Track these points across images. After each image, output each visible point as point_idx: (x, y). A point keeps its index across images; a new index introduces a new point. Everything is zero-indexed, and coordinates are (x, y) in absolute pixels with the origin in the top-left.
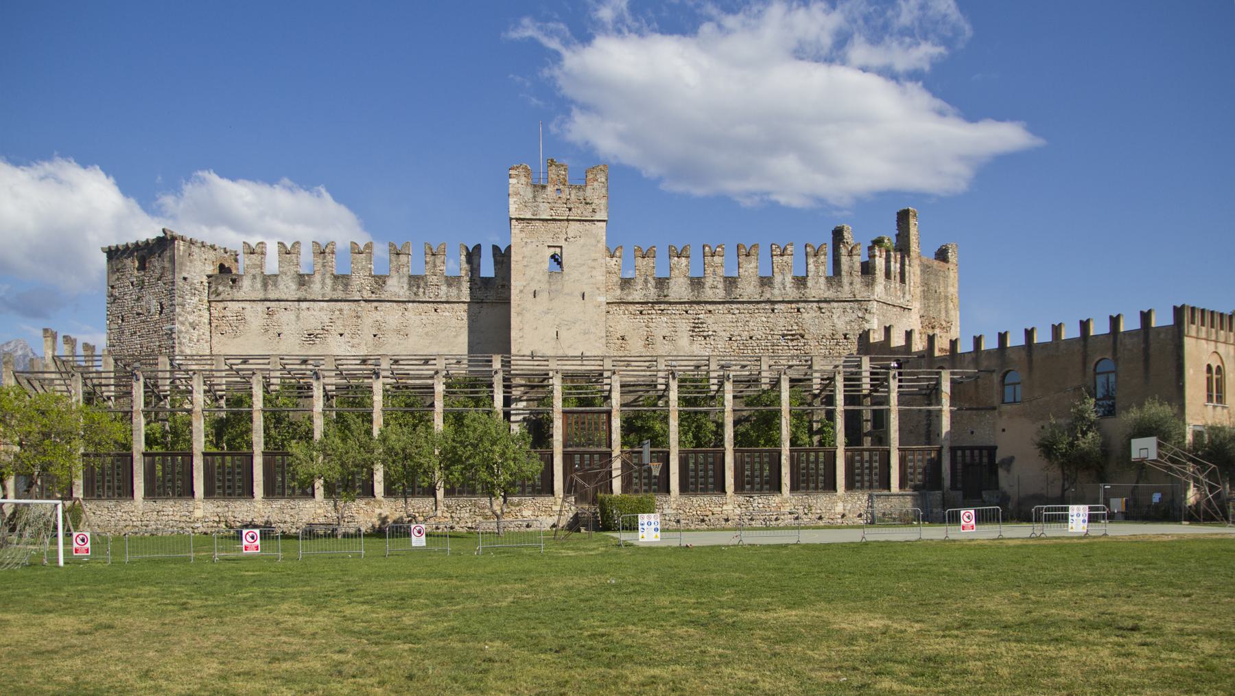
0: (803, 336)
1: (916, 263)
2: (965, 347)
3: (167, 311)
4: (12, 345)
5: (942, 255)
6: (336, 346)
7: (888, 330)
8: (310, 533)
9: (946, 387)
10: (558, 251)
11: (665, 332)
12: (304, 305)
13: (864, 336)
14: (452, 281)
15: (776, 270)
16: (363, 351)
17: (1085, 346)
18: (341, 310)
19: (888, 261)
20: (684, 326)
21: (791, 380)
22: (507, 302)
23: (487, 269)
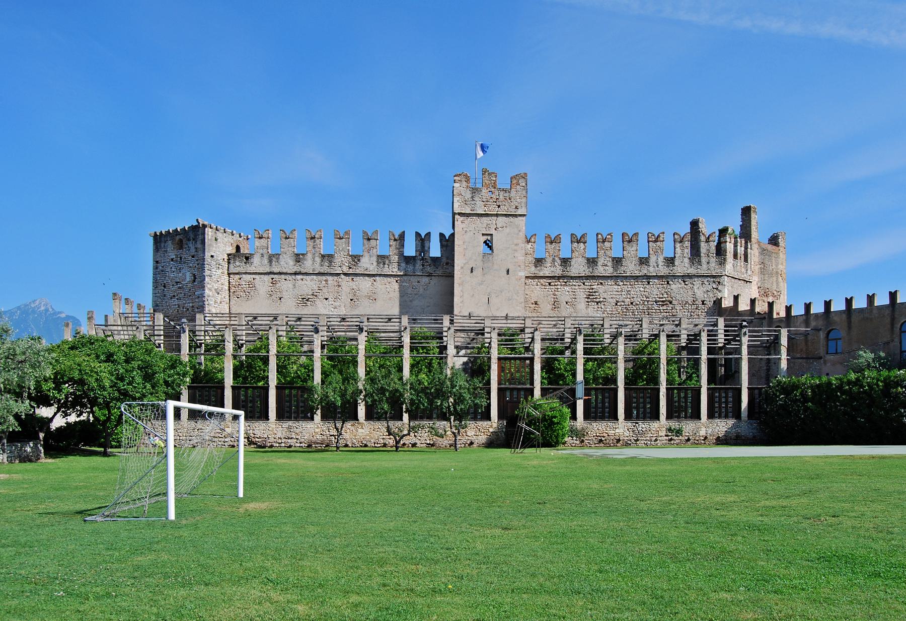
0: (671, 303)
1: (755, 246)
2: (798, 311)
3: (199, 280)
4: (37, 302)
5: (774, 240)
6: (322, 308)
7: (736, 298)
8: (310, 448)
9: (784, 341)
10: (489, 238)
11: (568, 299)
12: (299, 277)
13: (718, 302)
14: (382, 259)
15: (651, 252)
16: (343, 312)
17: (893, 311)
18: (326, 281)
19: (735, 246)
20: (581, 294)
21: (668, 336)
22: (451, 276)
23: (435, 251)
